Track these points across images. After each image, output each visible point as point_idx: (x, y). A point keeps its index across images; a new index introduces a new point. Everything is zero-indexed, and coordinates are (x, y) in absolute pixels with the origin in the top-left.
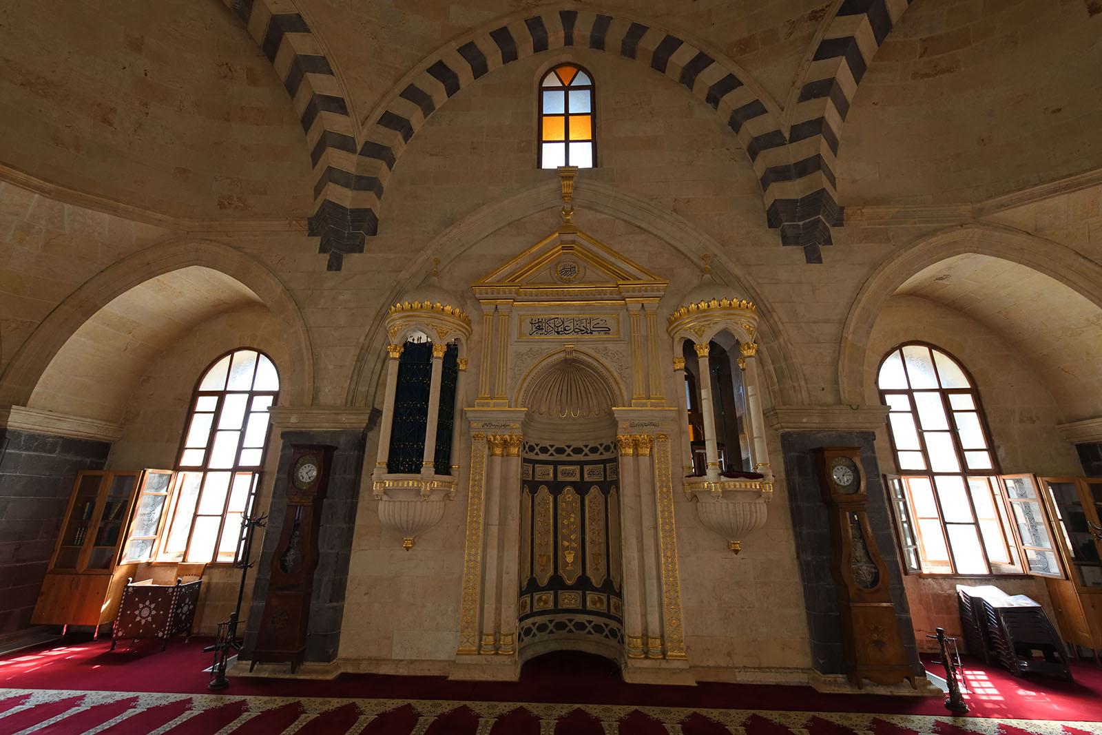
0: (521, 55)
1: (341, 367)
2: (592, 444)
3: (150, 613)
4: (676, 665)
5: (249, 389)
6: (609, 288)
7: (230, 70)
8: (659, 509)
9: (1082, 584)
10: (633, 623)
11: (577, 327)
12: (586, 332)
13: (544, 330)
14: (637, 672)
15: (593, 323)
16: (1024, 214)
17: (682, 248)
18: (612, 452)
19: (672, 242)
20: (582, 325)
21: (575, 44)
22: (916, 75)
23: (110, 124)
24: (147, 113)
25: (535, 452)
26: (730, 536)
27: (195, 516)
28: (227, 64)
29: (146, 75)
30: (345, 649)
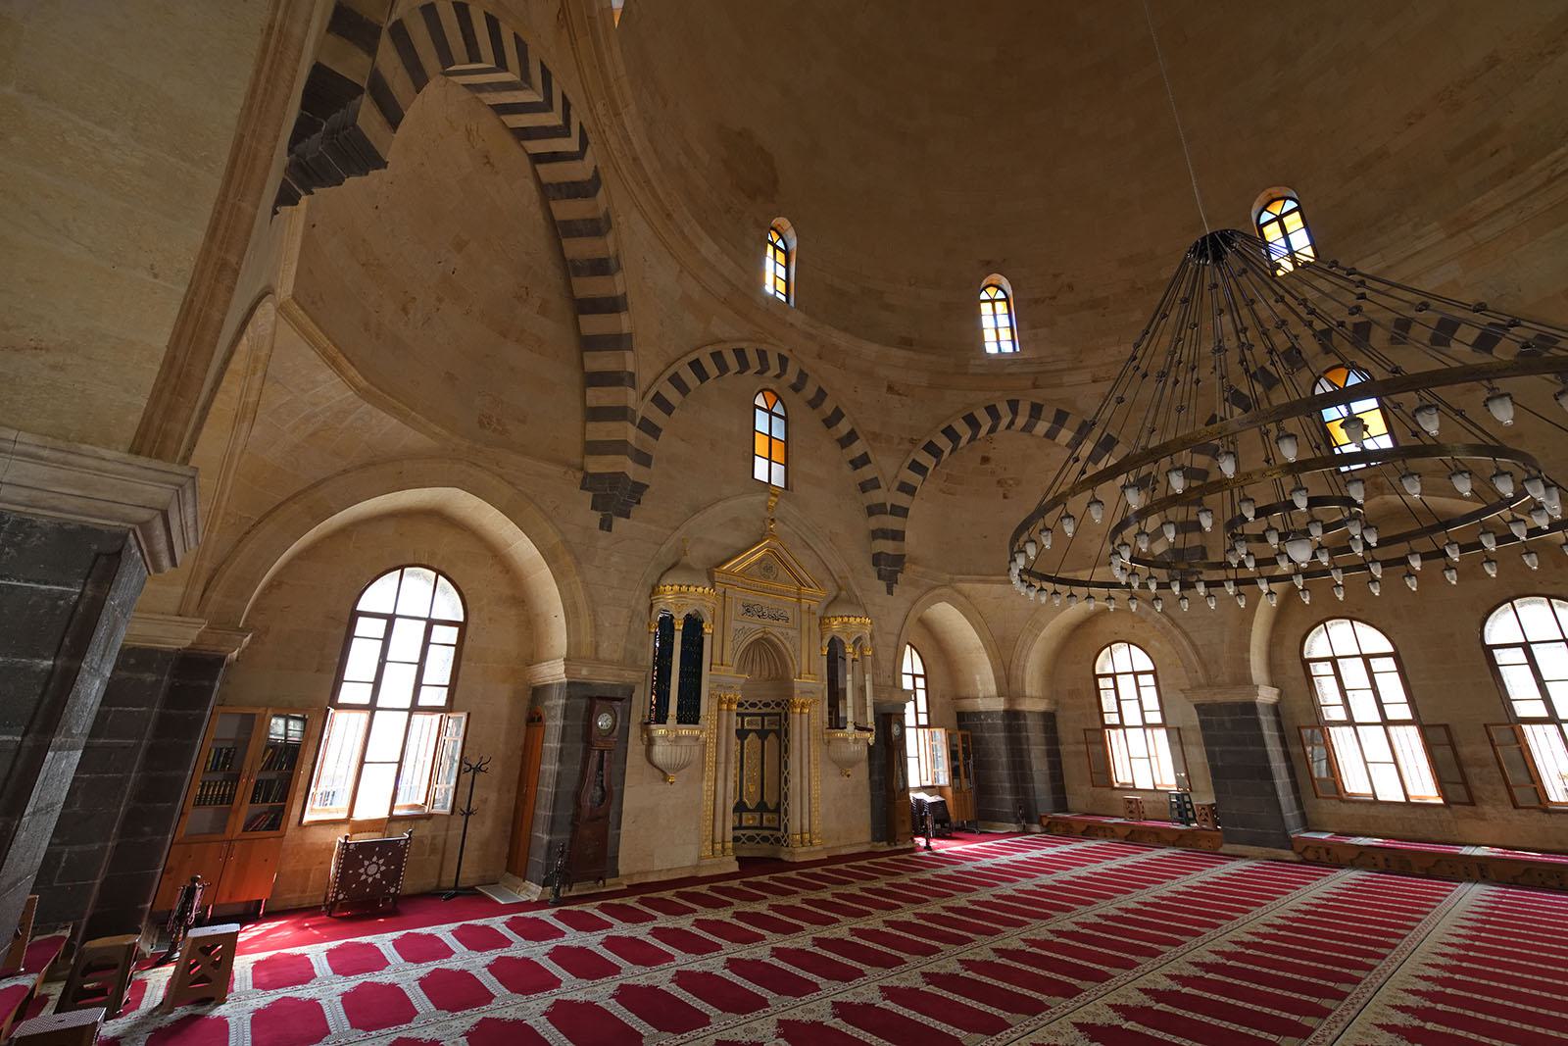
1: (616, 625)
3: (379, 869)
4: (818, 848)
5: (427, 616)
6: (794, 590)
7: (527, 294)
8: (812, 750)
9: (954, 792)
10: (794, 825)
14: (801, 855)
15: (780, 612)
16: (966, 587)
17: (831, 568)
19: (825, 561)
22: (941, 490)
23: (407, 313)
24: (438, 309)
26: (844, 766)
27: (362, 762)
28: (527, 288)
29: (453, 273)
30: (622, 869)
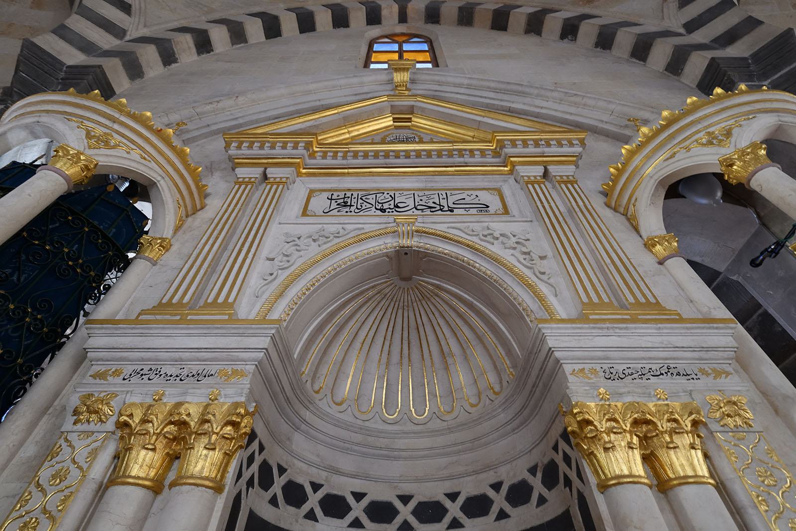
0: (353, 23)
2: (469, 488)
11: (421, 203)
12: (441, 210)
13: (353, 209)
18: (542, 500)
20: (433, 200)
21: (409, 20)
25: (306, 508)
